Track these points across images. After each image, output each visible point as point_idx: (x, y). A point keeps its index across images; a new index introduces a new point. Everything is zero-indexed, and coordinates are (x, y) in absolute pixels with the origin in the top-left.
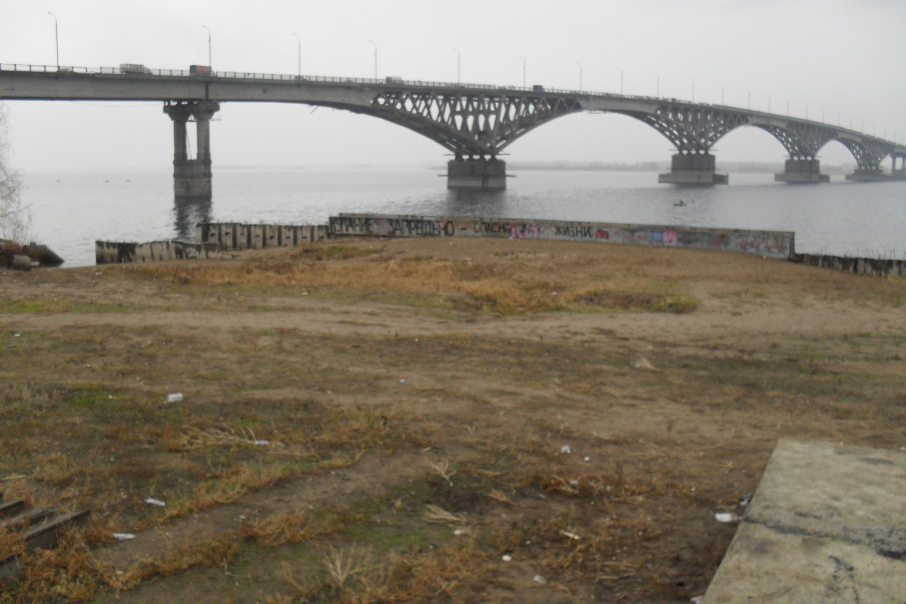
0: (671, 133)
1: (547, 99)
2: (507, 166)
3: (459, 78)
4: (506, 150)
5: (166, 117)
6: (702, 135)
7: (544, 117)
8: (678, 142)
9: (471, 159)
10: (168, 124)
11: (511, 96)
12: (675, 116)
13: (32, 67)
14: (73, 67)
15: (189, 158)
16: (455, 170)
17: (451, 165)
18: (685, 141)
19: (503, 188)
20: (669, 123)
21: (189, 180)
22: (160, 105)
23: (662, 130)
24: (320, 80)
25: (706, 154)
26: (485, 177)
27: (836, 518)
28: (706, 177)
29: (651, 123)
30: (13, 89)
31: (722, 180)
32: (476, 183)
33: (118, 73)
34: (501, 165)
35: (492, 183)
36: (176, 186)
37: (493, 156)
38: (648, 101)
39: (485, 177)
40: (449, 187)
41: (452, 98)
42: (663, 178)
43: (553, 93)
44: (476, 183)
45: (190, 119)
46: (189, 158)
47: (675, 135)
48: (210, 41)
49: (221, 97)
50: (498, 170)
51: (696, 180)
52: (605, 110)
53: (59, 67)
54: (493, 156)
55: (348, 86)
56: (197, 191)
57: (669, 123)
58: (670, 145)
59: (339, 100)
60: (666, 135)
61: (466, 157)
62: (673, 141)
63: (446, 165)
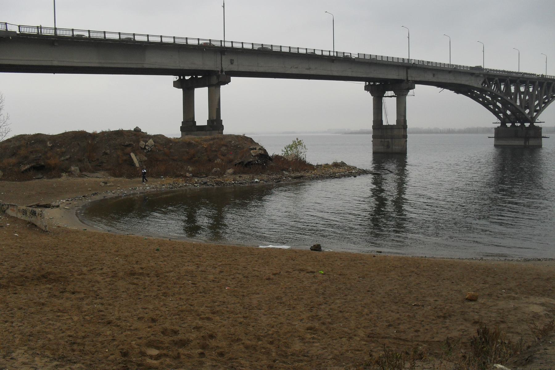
1: (499, 79)
3: (367, 133)
5: (368, 94)
8: (501, 115)
10: (369, 98)
13: (282, 48)
14: (134, 35)
15: (384, 124)
17: (497, 130)
18: (508, 112)
19: (540, 146)
21: (390, 140)
22: (362, 84)
23: (486, 105)
24: (395, 61)
26: (527, 138)
27: (440, 356)
29: (475, 98)
30: (309, 69)
33: (392, 124)
34: (539, 129)
35: (532, 142)
36: (374, 145)
40: (496, 146)
45: (386, 95)
46: (384, 124)
47: (498, 107)
48: (224, 7)
49: (234, 68)
53: (55, 29)
55: (454, 71)
56: (396, 148)
58: (495, 119)
60: (489, 109)
61: (509, 125)
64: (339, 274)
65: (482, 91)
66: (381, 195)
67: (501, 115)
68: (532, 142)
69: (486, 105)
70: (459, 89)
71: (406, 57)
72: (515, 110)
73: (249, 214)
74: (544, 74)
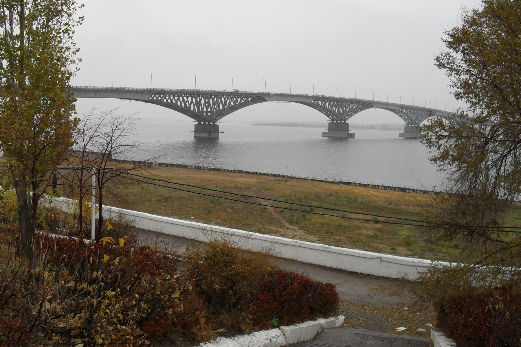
0: (405, 117)
2: (350, 125)
4: (349, 119)
6: (416, 119)
7: (362, 109)
8: (407, 121)
9: (205, 123)
11: (229, 95)
12: (406, 111)
16: (197, 129)
17: (330, 123)
20: (404, 114)
23: (401, 117)
25: (345, 122)
26: (210, 133)
28: (344, 135)
29: (397, 114)
31: (352, 136)
32: (206, 135)
34: (348, 124)
35: (213, 135)
37: (214, 123)
38: (397, 105)
39: (210, 133)
40: (195, 137)
41: (3, 85)
42: (324, 134)
43: (157, 90)
44: (206, 135)
50: (216, 129)
51: (339, 136)
52: (382, 108)
54: (214, 123)
57: (404, 114)
59: (301, 101)
60: (403, 118)
62: (405, 121)
63: (328, 125)
64: (265, 338)
65: (400, 111)
66: (499, 139)
67: (407, 121)
68: (213, 135)
69: (401, 117)
70: (392, 110)
71: (372, 100)
72: (411, 120)
73: (168, 195)
74: (335, 96)
